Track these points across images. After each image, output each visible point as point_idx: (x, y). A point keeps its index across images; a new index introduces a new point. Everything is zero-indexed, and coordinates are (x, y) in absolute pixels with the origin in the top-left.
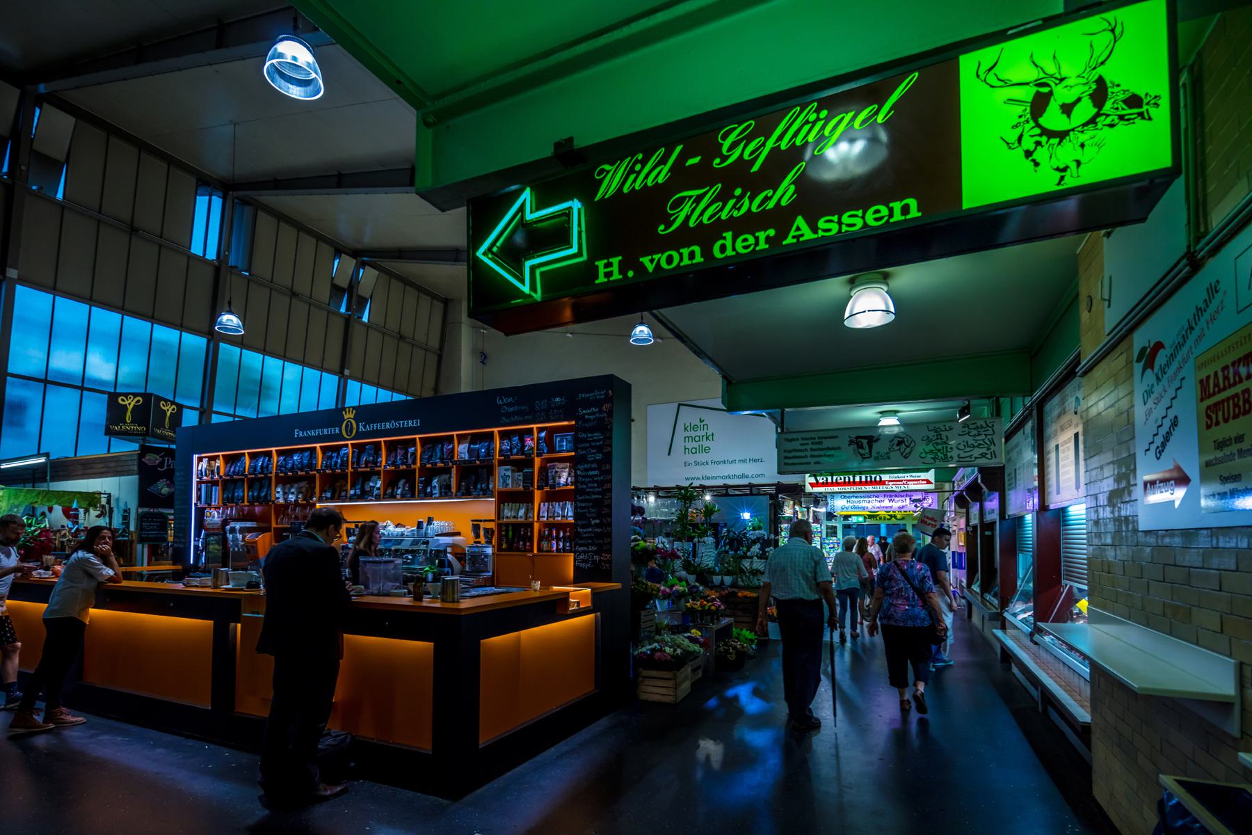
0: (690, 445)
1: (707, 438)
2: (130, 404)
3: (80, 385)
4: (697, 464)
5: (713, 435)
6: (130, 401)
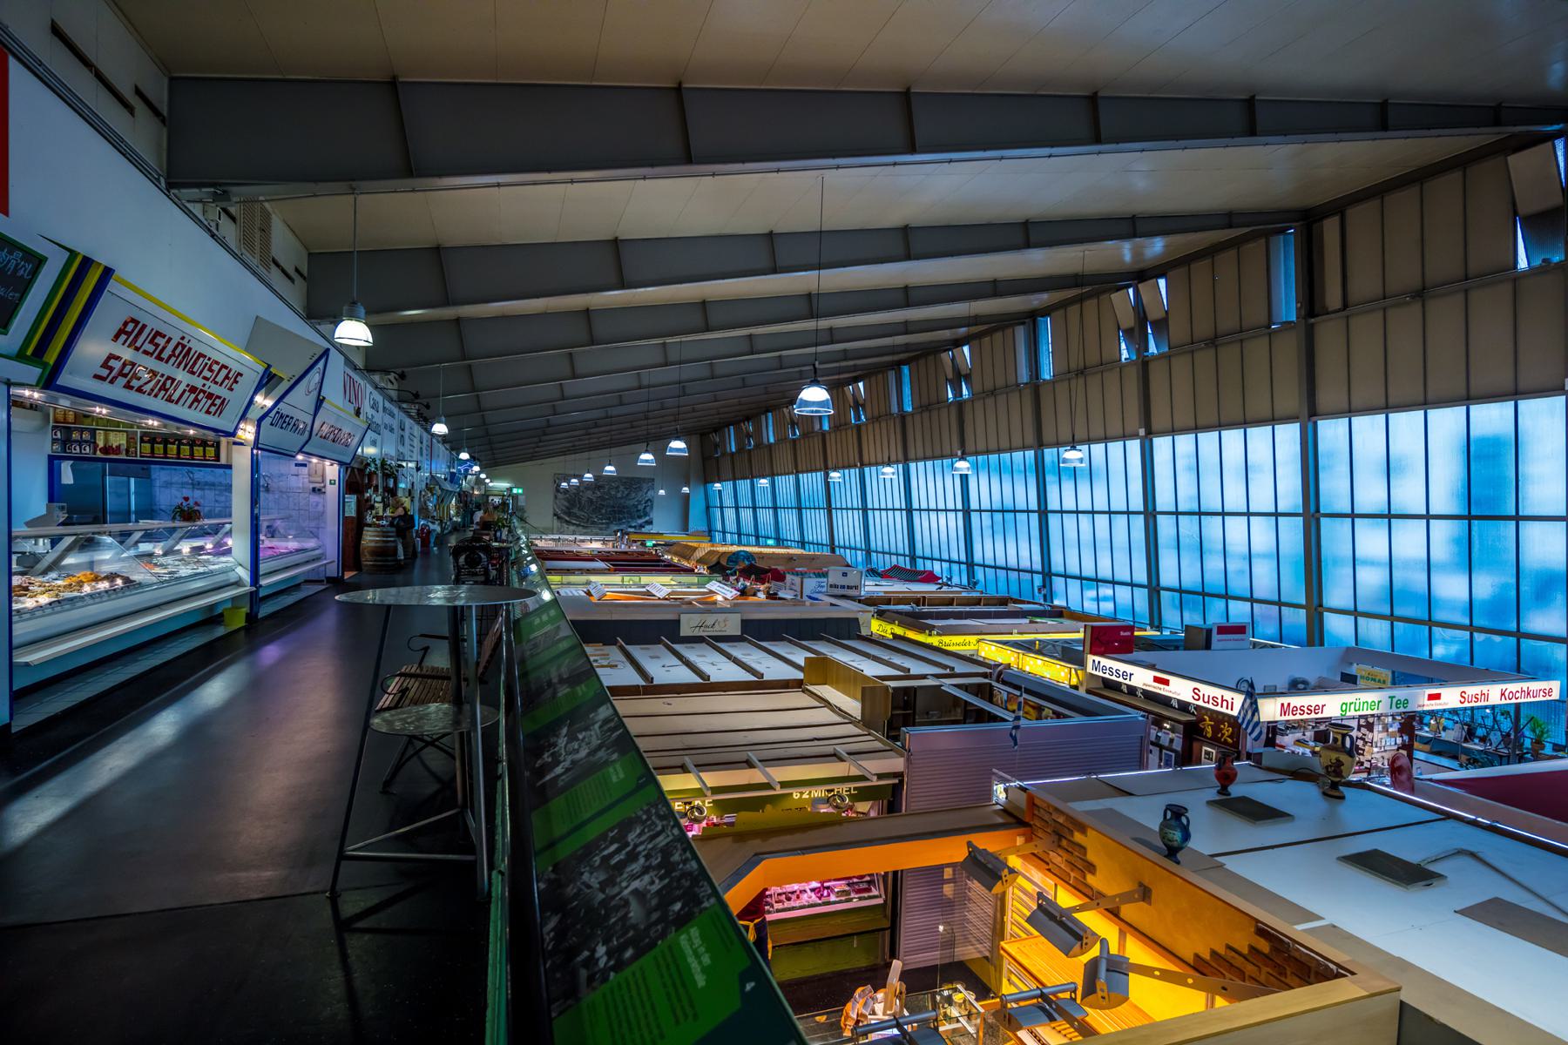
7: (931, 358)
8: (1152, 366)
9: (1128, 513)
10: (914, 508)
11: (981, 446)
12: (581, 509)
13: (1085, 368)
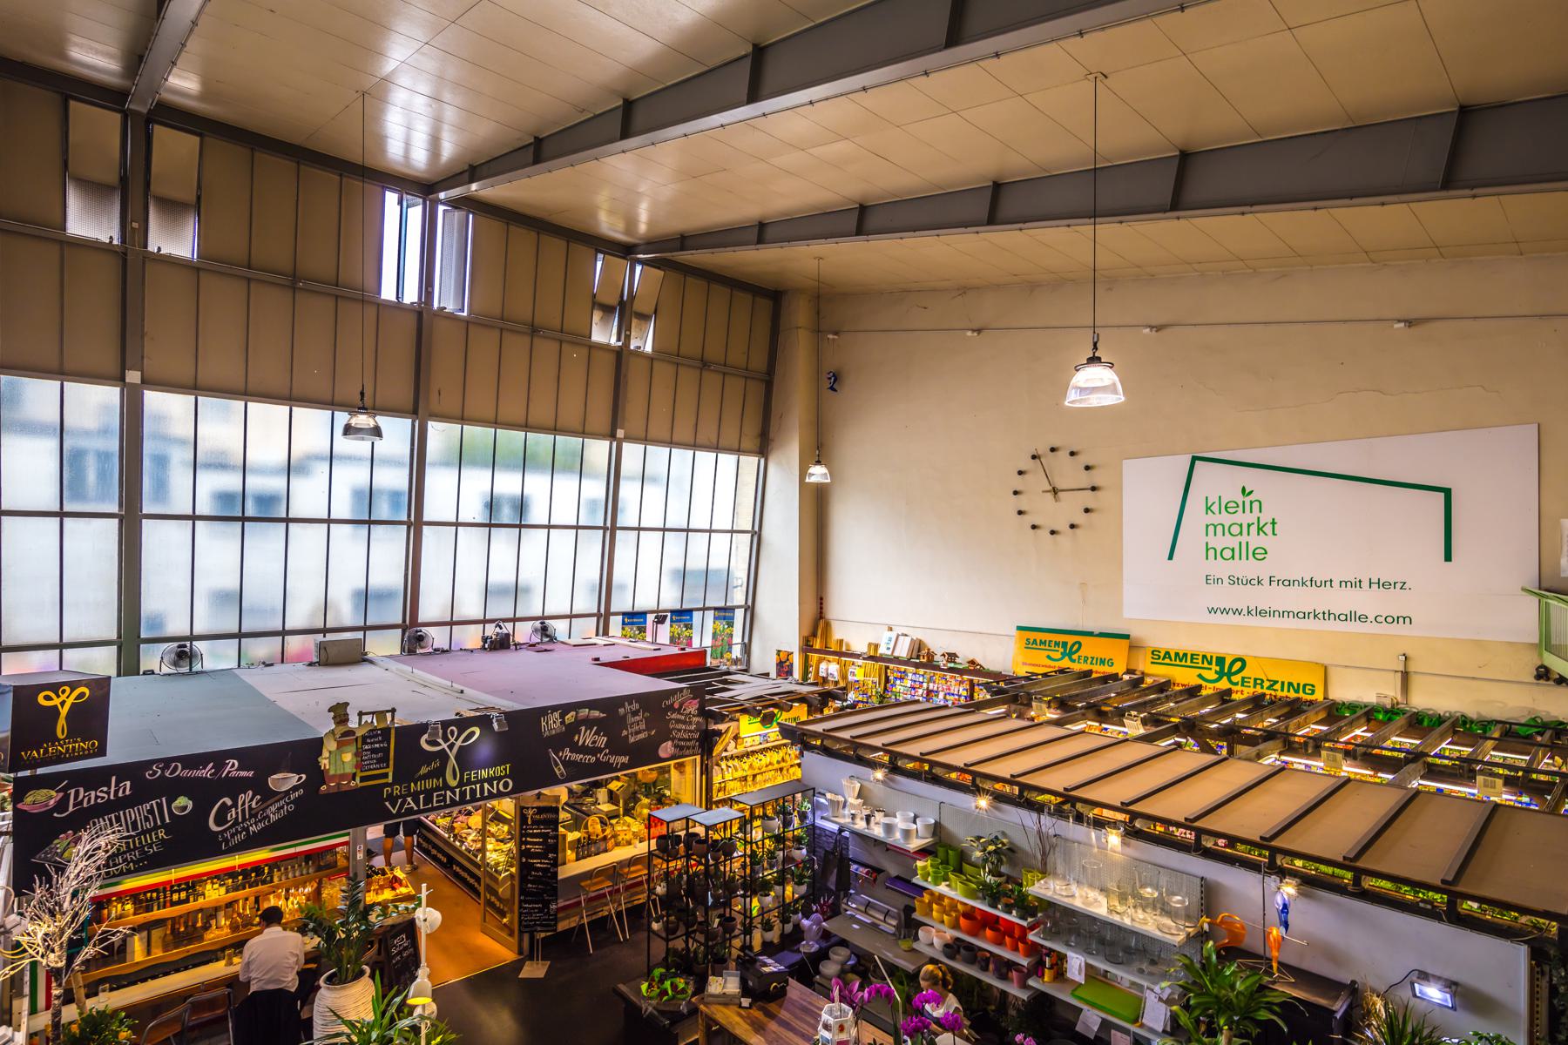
0: (1219, 542)
1: (1260, 529)
2: (63, 703)
3: (241, 515)
4: (1235, 581)
5: (1273, 523)
6: (63, 697)
13: (532, 326)
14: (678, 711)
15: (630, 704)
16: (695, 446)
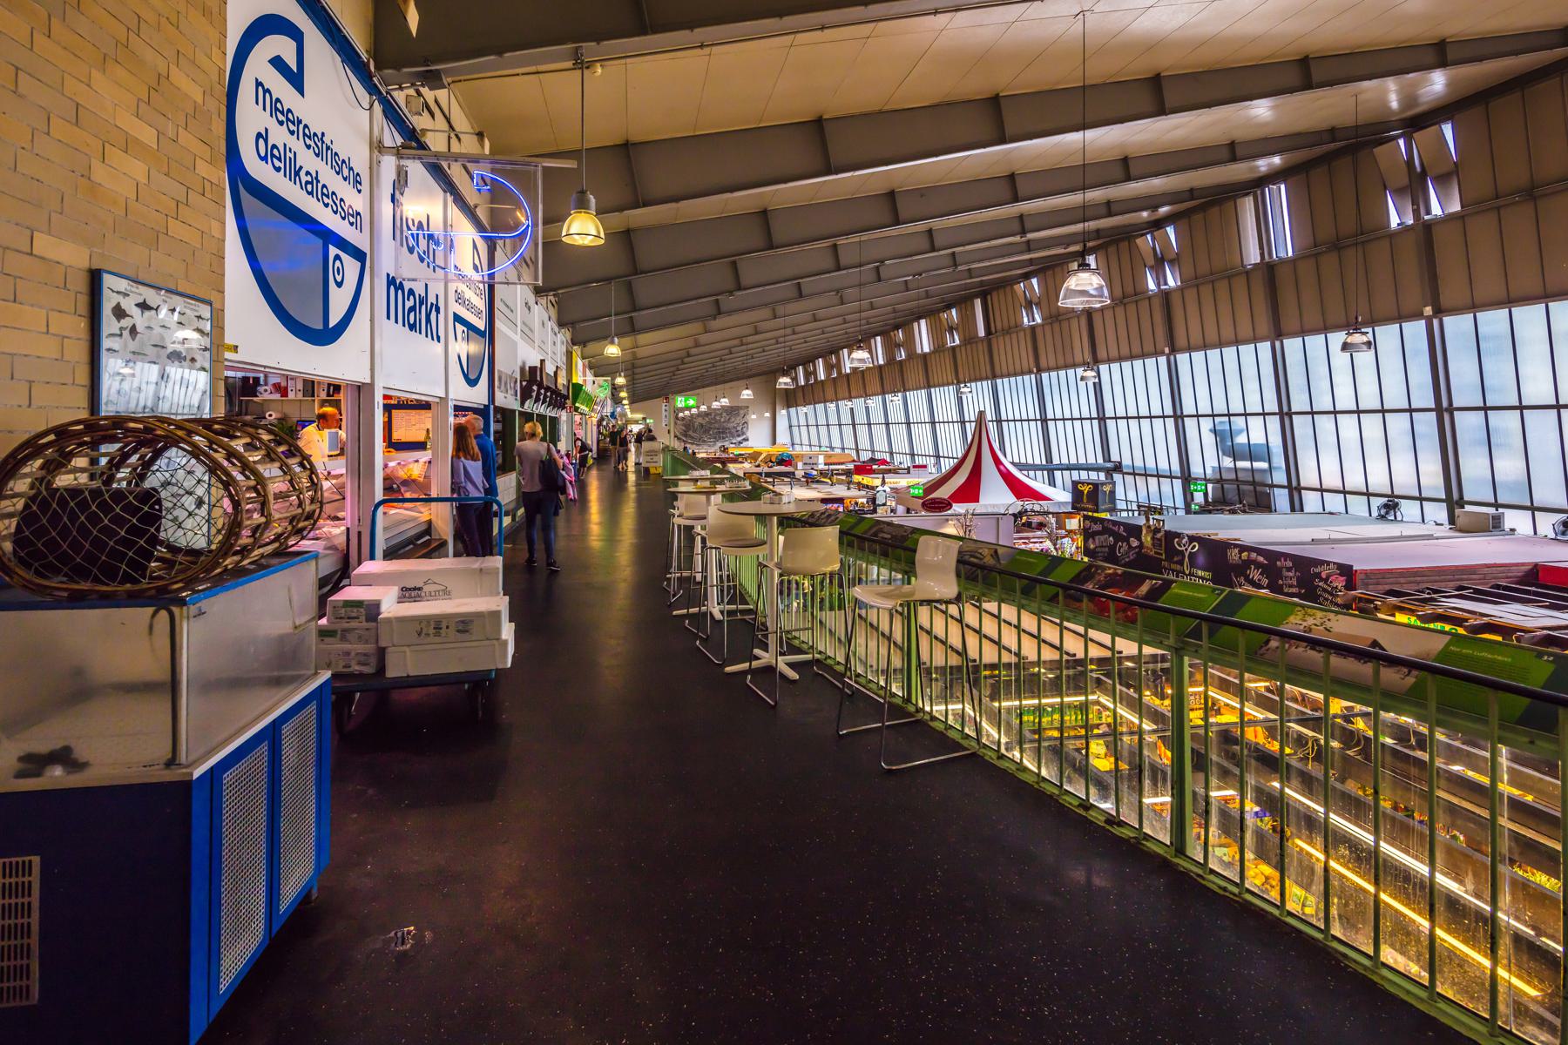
7: (1124, 245)
8: (1436, 232)
9: (1116, 418)
10: (1048, 417)
11: (1052, 363)
12: (695, 431)
14: (1326, 580)
15: (1285, 560)
16: (1509, 302)
